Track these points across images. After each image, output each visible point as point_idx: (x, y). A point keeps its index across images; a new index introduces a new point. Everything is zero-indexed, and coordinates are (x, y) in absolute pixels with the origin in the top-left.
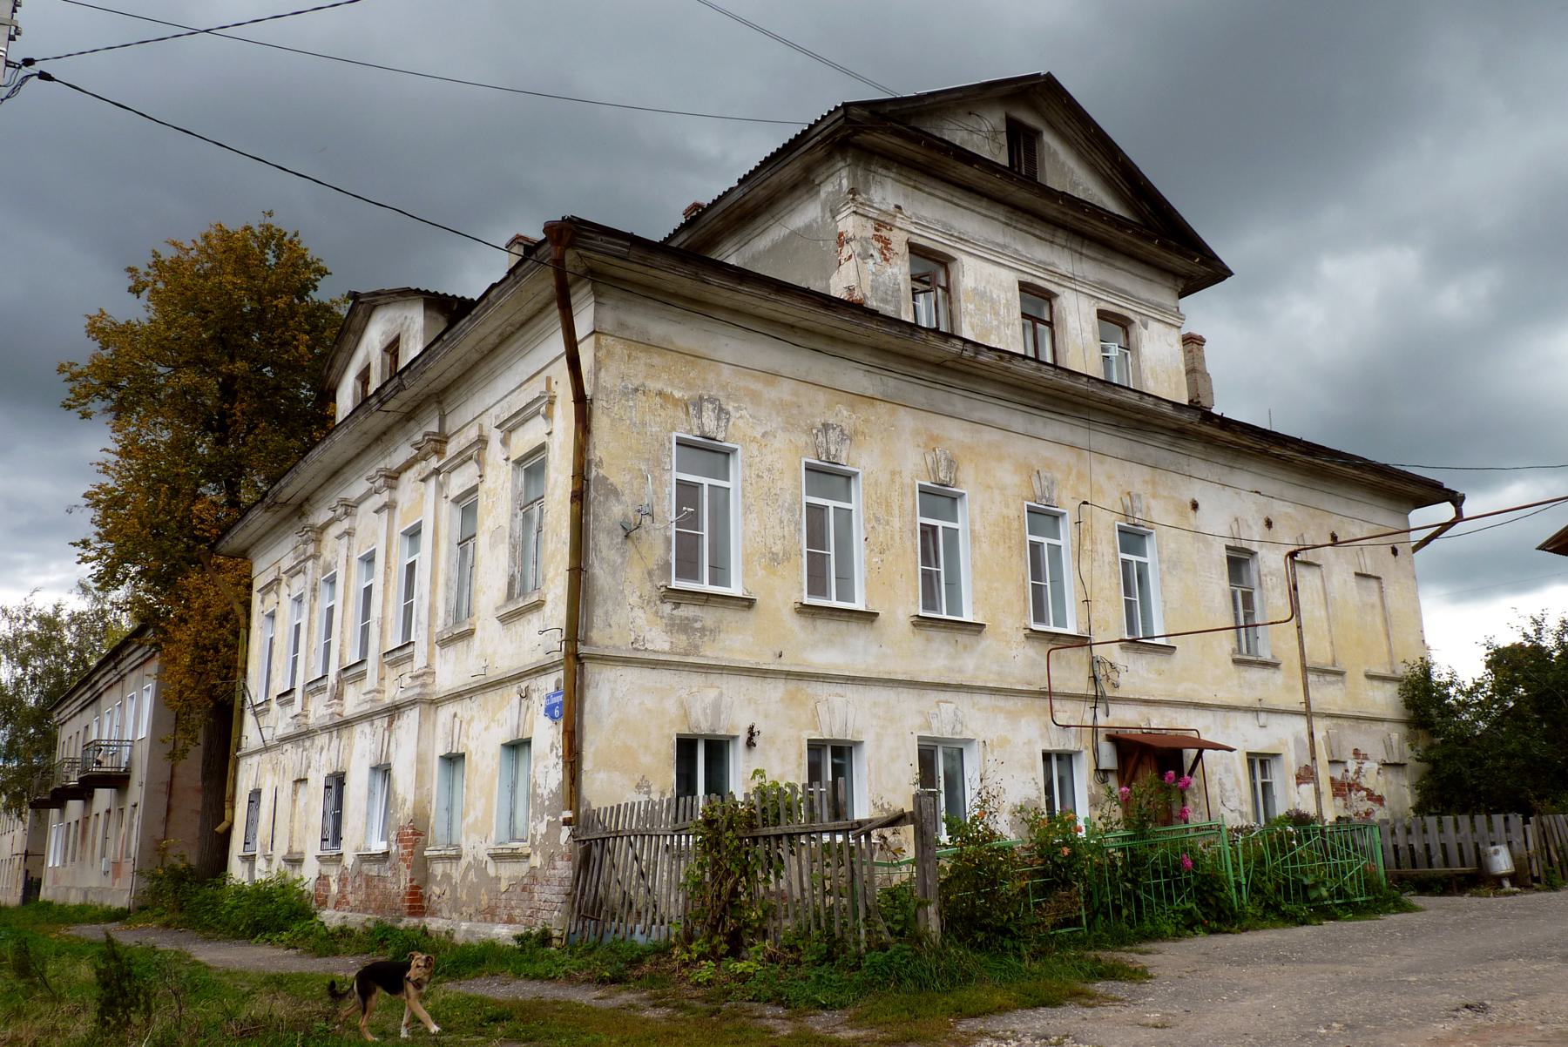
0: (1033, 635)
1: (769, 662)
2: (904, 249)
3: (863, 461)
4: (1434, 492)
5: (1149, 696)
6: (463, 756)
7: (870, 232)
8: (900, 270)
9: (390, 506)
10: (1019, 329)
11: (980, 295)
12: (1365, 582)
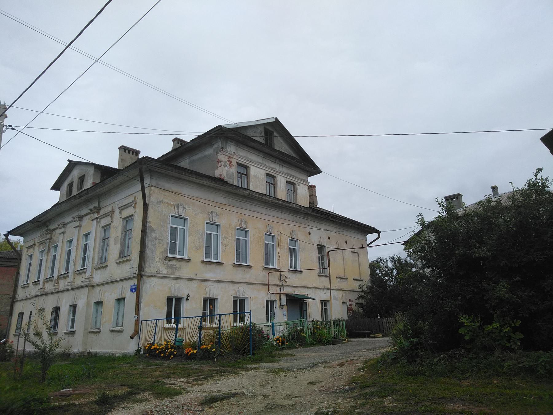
0: (265, 268)
1: (193, 276)
2: (235, 164)
3: (222, 221)
4: (372, 230)
5: (296, 284)
6: (102, 302)
7: (226, 160)
8: (234, 170)
9: (79, 226)
10: (265, 186)
11: (255, 176)
12: (354, 254)
